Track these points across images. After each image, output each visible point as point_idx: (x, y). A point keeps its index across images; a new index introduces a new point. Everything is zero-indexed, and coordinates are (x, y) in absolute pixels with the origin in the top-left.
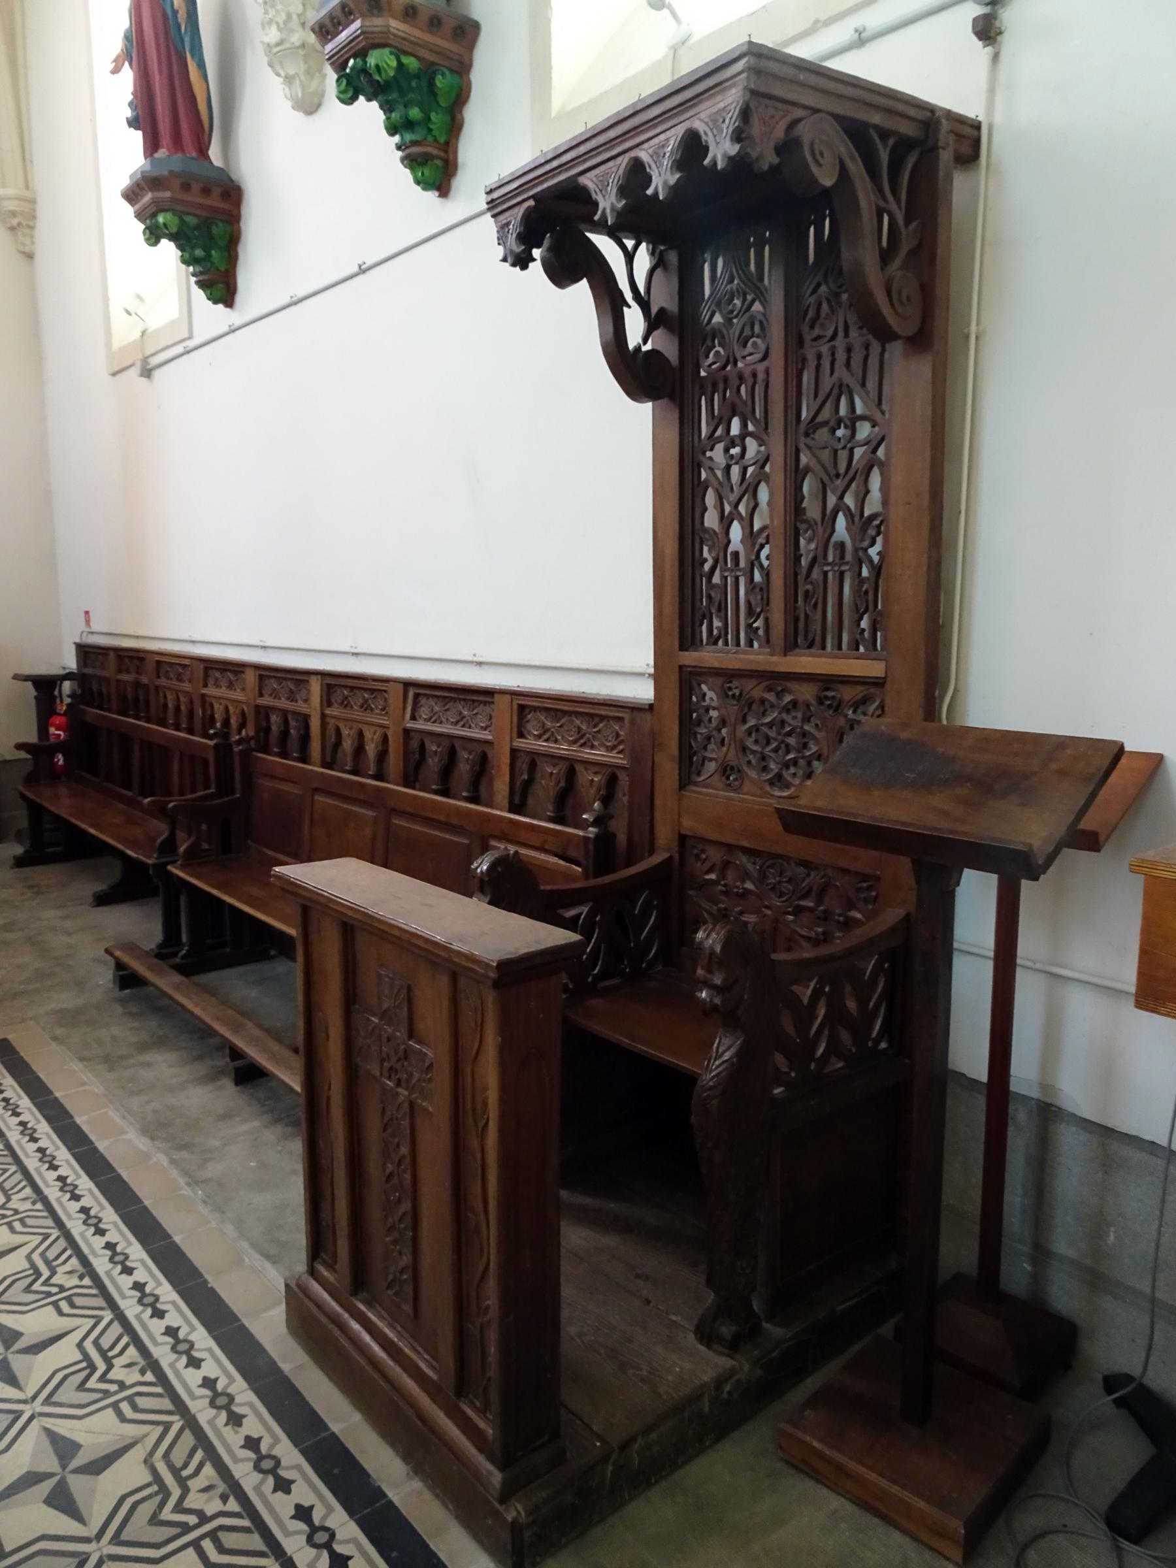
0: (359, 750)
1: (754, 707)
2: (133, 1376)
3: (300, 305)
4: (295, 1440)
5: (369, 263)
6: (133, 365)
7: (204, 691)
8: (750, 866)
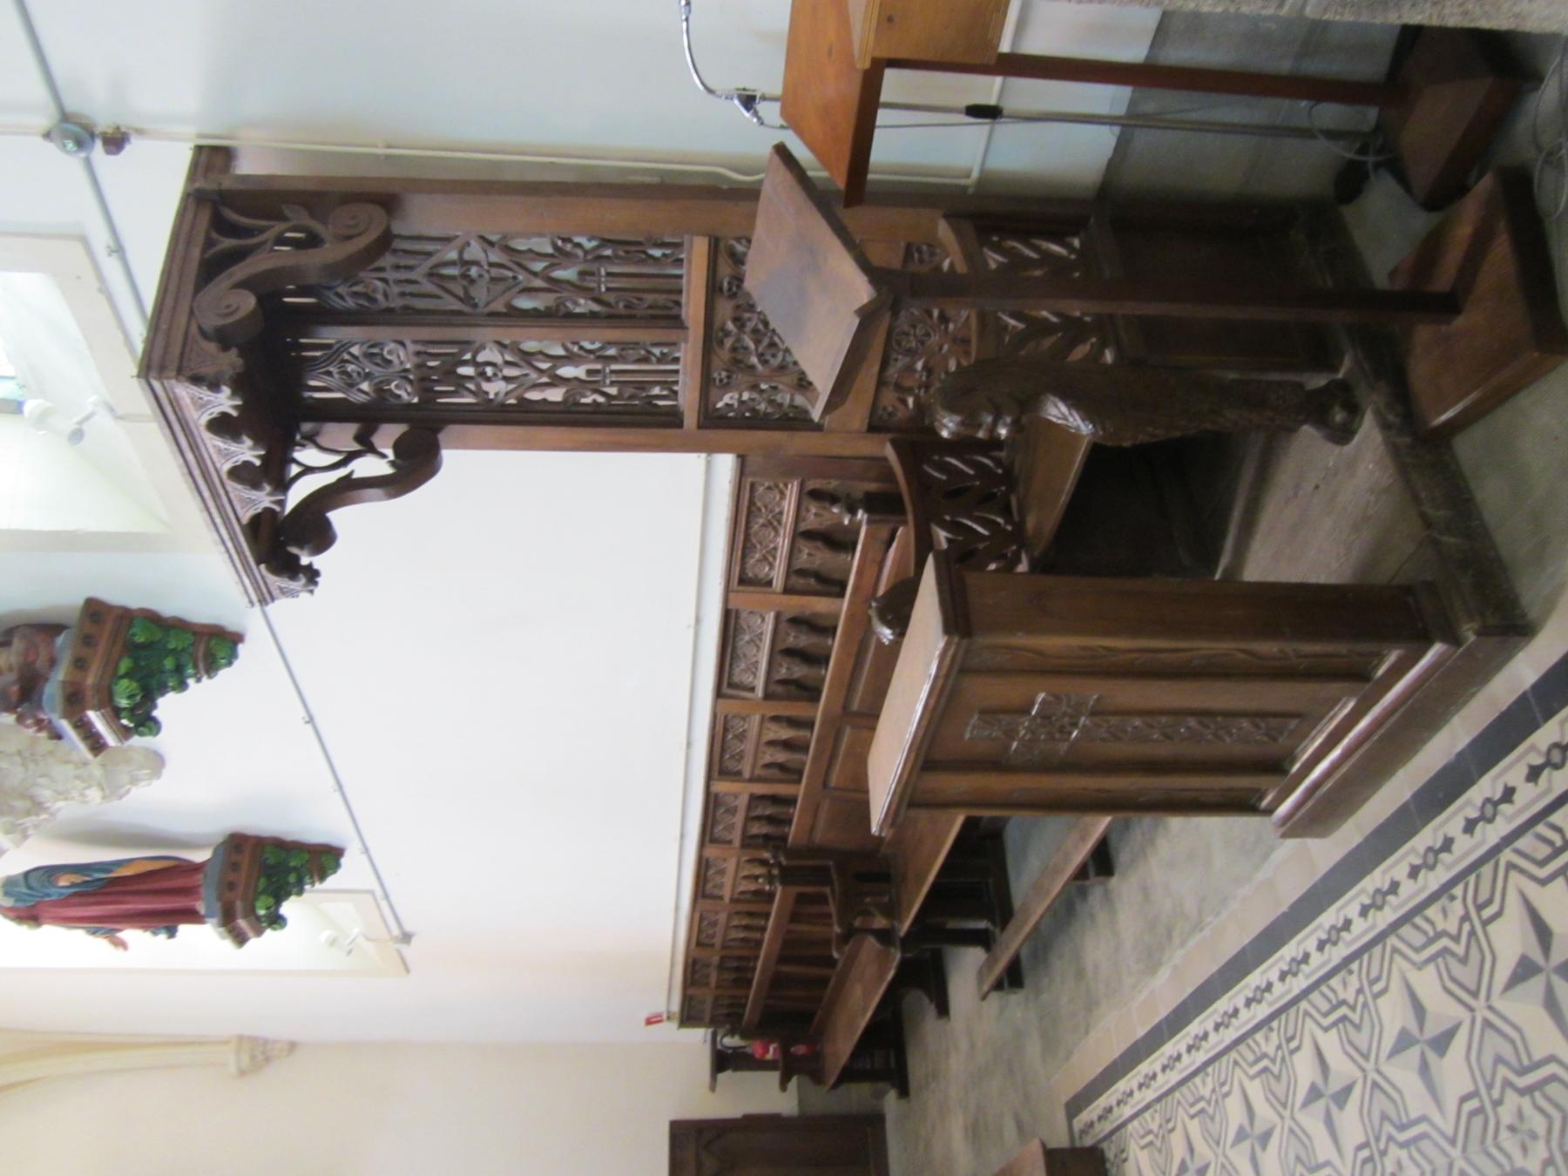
0: (787, 745)
1: (739, 357)
2: (1354, 982)
3: (343, 782)
4: (1413, 833)
5: (303, 713)
6: (399, 951)
7: (727, 899)
8: (900, 364)
